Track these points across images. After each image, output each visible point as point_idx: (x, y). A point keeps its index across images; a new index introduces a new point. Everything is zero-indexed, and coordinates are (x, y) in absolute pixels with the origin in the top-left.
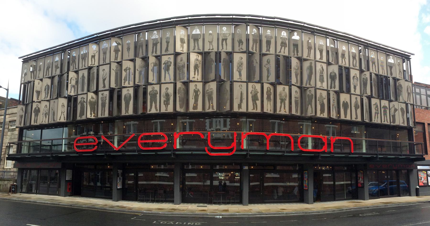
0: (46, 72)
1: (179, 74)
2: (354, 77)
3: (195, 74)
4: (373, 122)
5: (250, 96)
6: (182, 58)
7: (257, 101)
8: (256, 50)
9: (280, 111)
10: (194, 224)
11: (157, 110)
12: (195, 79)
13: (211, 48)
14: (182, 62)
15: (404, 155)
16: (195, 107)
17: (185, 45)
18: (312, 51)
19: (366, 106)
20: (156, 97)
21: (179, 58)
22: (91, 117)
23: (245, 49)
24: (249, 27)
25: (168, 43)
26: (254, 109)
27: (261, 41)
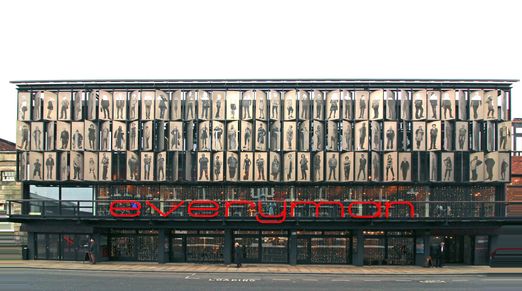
0: (62, 113)
1: (230, 142)
2: (417, 131)
3: (246, 144)
4: (443, 181)
5: (299, 165)
6: (232, 126)
7: (306, 171)
8: (306, 118)
9: (330, 178)
10: (249, 280)
11: (207, 179)
12: (246, 149)
13: (262, 117)
14: (233, 130)
15: (469, 219)
16: (246, 177)
17: (237, 111)
18: (366, 110)
19: (433, 163)
20: (206, 165)
21: (230, 125)
22: (132, 179)
23: (295, 118)
24: (299, 92)
25: (219, 107)
26: (303, 178)
27: (312, 107)
